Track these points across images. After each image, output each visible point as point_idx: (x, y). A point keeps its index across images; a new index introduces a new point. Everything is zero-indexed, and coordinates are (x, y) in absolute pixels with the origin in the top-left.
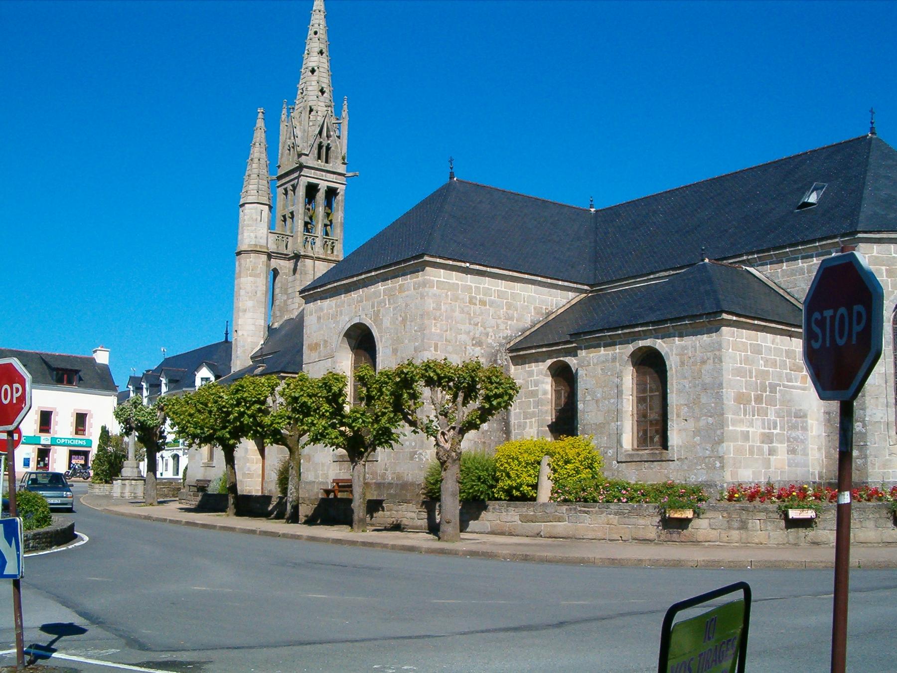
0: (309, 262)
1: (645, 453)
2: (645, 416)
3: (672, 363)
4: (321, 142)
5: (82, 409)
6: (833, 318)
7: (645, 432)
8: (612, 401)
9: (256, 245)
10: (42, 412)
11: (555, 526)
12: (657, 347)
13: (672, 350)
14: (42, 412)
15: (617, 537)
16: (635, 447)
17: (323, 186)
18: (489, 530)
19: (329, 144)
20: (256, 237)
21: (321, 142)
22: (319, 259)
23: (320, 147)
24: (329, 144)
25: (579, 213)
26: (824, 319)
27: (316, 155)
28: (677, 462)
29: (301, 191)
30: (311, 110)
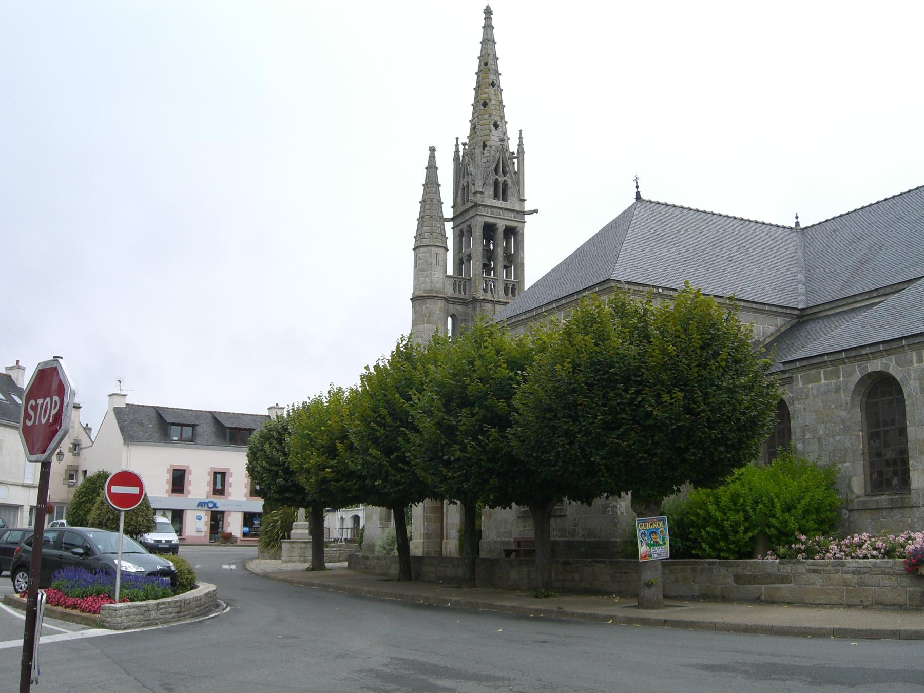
0: (488, 306)
1: (884, 499)
2: (879, 455)
3: (911, 388)
4: (497, 179)
5: (180, 463)
6: (42, 405)
7: (880, 474)
8: (838, 438)
9: (431, 291)
10: (174, 470)
11: (778, 588)
12: (891, 371)
13: (909, 375)
14: (174, 470)
15: (856, 601)
16: (869, 490)
17: (501, 225)
18: (697, 593)
19: (505, 181)
20: (431, 282)
21: (497, 179)
22: (499, 303)
23: (496, 183)
24: (505, 181)
25: (414, 307)
26: (37, 405)
27: (492, 193)
28: (923, 509)
29: (478, 232)
30: (484, 146)
